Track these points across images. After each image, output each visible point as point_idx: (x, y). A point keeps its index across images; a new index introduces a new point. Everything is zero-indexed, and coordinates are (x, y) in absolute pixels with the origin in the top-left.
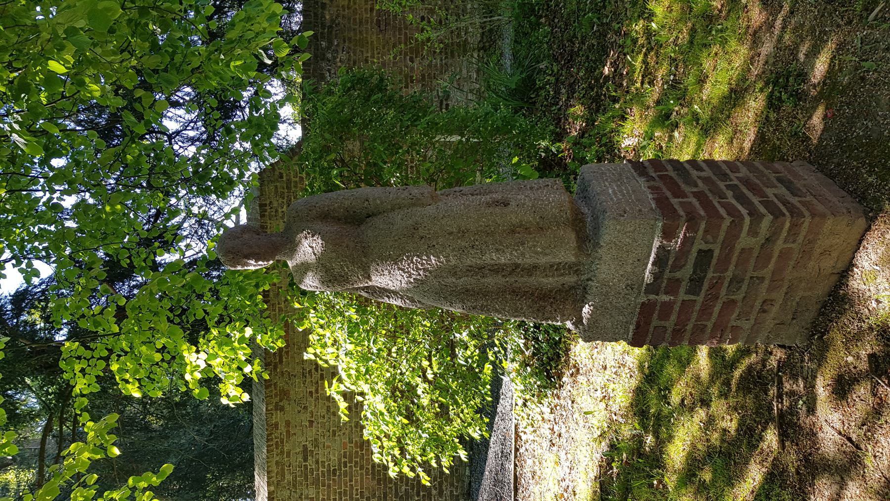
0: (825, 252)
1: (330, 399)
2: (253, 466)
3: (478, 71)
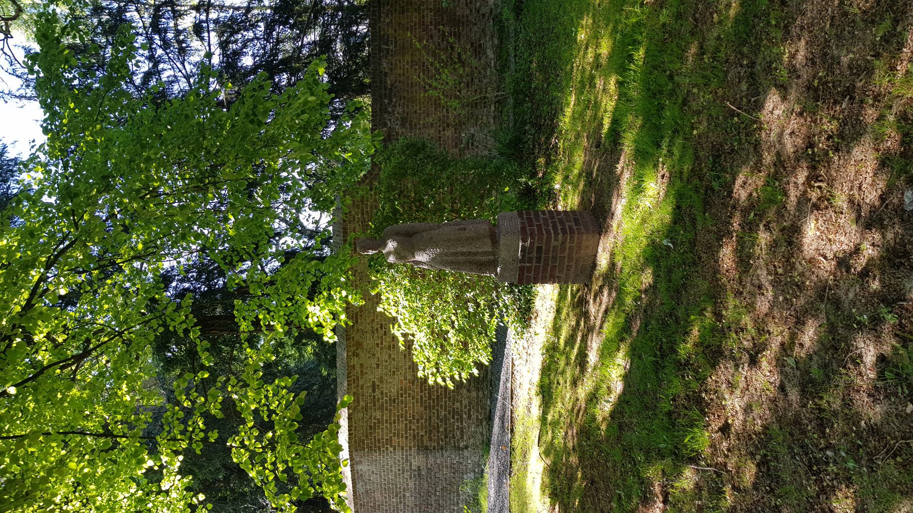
1: (394, 338)
3: (494, 118)
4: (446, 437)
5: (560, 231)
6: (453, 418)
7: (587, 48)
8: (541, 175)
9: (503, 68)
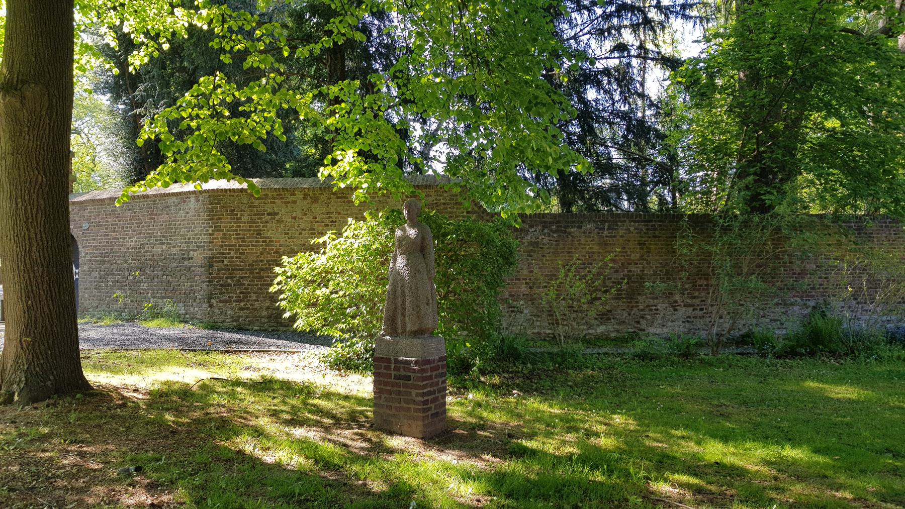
0: (410, 426)
3: (539, 333)
4: (222, 286)
5: (426, 398)
6: (241, 293)
7: (606, 424)
8: (482, 379)
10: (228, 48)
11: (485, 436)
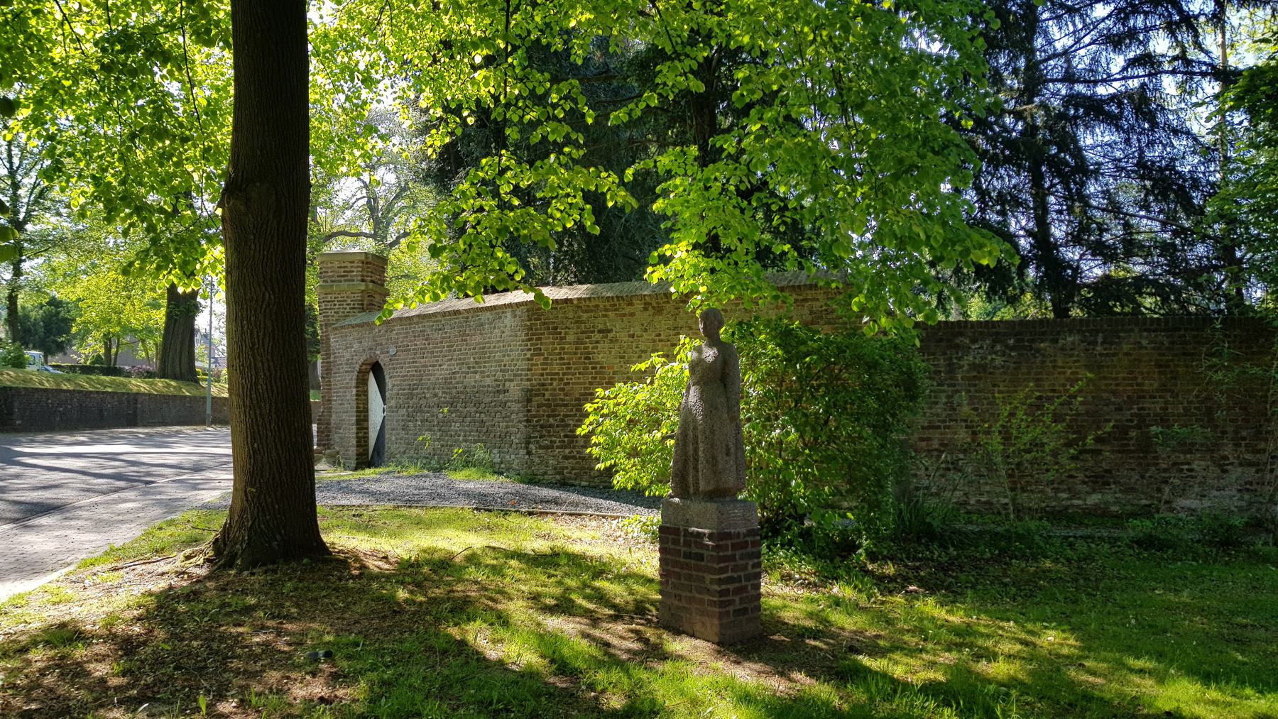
2: (597, 281)
3: (989, 503)
4: (542, 426)
5: (723, 587)
6: (566, 436)
7: (1026, 643)
8: (870, 567)
9: (1057, 516)
10: (515, 119)
11: (815, 647)
